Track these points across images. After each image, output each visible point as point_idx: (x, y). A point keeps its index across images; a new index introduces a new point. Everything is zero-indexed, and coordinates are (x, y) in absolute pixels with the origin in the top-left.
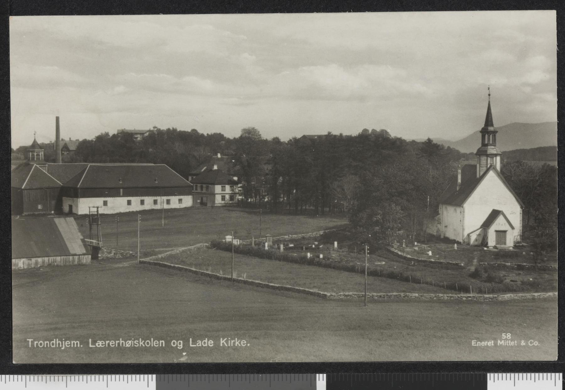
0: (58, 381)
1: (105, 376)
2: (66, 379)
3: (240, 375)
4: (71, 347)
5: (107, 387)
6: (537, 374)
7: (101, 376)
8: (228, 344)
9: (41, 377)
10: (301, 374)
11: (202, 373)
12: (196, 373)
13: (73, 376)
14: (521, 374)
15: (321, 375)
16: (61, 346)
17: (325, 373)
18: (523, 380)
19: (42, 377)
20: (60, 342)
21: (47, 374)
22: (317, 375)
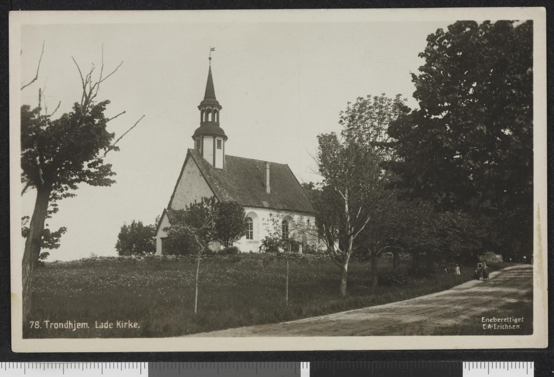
0: (56, 368)
1: (100, 363)
6: (510, 363)
7: (96, 364)
10: (286, 362)
11: (192, 361)
13: (69, 364)
14: (494, 363)
15: (305, 363)
17: (309, 361)
18: (500, 368)
20: (72, 324)
21: (45, 362)
22: (302, 363)
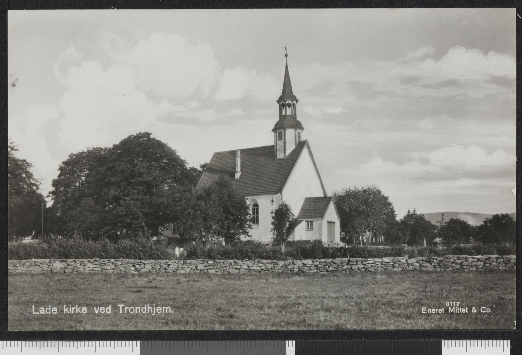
1: (94, 342)
2: (35, 344)
3: (216, 342)
4: (427, 312)
5: (96, 352)
6: (487, 341)
7: (90, 342)
8: (69, 312)
9: (35, 343)
12: (177, 340)
13: (64, 342)
14: (472, 341)
15: (290, 342)
16: (152, 312)
19: (36, 343)
